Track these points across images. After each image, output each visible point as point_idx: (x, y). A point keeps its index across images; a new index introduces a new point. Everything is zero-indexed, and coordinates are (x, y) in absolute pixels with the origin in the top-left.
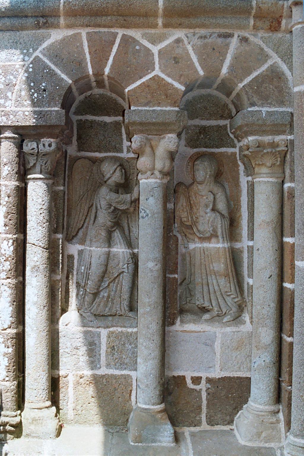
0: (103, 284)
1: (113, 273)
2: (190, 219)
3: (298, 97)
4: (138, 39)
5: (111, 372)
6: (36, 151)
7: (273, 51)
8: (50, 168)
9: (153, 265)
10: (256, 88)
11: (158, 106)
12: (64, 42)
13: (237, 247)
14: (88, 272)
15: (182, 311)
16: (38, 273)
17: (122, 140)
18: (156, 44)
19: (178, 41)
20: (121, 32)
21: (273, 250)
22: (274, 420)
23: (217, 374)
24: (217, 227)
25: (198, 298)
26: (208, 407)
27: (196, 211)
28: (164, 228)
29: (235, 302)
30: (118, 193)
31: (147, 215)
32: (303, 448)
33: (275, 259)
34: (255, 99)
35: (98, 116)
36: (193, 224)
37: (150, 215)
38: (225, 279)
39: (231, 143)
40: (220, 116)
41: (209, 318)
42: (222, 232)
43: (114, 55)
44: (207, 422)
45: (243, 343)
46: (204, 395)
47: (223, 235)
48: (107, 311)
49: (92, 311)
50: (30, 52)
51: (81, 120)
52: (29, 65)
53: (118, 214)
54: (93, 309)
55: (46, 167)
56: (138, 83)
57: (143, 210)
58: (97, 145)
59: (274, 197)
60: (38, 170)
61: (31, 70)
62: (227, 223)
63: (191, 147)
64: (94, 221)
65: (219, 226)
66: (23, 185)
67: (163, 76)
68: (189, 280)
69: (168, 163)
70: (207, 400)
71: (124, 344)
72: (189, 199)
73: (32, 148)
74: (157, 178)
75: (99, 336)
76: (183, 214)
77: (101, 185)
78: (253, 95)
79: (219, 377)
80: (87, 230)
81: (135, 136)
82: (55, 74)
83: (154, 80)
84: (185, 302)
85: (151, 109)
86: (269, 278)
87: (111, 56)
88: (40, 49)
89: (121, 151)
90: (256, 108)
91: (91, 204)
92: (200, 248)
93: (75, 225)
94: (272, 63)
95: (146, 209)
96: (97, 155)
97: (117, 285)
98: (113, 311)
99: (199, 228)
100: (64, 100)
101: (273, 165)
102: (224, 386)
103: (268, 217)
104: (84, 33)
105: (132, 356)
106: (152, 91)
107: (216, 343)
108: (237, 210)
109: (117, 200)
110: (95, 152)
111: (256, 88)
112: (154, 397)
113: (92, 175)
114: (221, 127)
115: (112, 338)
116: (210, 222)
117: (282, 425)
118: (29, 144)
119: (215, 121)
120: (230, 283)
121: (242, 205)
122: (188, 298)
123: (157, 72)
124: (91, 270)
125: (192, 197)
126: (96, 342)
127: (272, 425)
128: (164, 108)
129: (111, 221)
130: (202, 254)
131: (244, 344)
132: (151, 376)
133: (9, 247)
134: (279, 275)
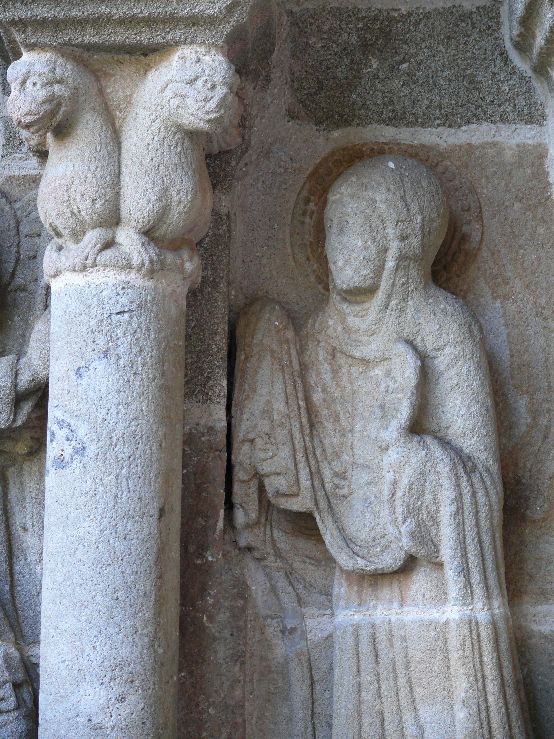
9: (102, 701)
24: (435, 520)
27: (335, 441)
28: (162, 512)
31: (81, 451)
36: (323, 504)
37: (91, 450)
39: (521, 101)
42: (462, 543)
47: (465, 556)
57: (61, 424)
62: (489, 498)
65: (446, 511)
69: (182, 192)
72: (301, 380)
74: (128, 266)
76: (271, 454)
81: (27, 57)
92: (357, 628)
95: (73, 422)
108: (546, 437)
114: (466, 17)
116: (399, 494)
125: (319, 374)
130: (367, 662)
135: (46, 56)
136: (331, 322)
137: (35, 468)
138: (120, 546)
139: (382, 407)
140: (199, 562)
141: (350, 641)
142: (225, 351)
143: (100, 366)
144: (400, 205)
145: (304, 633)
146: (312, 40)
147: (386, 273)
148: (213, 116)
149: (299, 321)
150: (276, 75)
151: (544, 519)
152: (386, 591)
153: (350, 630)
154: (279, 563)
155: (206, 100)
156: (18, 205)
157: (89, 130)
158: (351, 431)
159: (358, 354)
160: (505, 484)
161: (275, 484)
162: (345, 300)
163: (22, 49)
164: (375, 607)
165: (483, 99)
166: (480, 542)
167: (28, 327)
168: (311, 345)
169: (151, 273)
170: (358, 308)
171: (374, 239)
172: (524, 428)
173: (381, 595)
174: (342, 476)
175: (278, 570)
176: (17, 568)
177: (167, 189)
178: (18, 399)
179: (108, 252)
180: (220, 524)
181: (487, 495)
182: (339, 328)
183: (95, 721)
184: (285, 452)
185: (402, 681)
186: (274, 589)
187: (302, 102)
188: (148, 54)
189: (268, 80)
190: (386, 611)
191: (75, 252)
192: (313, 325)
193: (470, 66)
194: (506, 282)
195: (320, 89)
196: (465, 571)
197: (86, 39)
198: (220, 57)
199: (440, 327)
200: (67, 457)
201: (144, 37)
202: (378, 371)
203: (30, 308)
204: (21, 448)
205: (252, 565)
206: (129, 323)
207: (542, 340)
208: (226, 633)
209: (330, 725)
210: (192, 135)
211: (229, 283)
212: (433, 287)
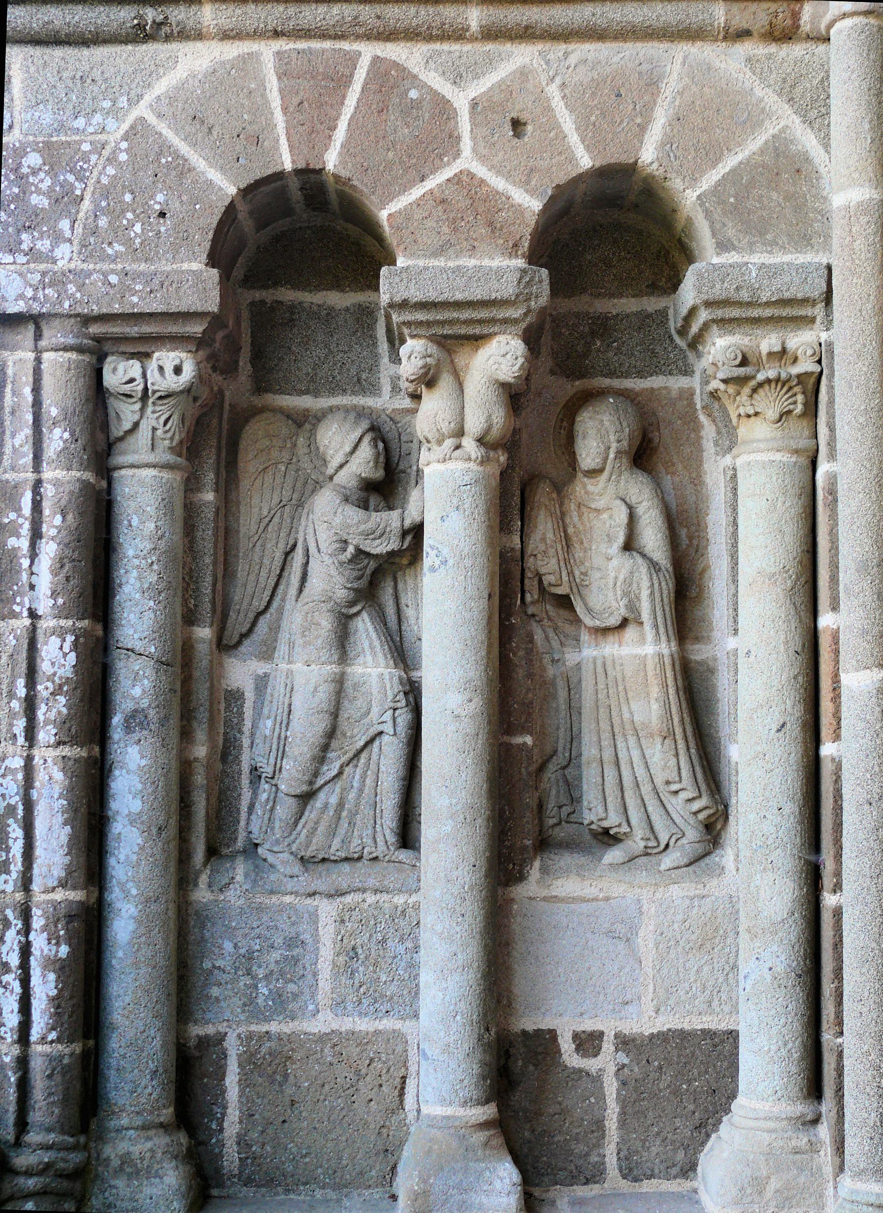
0: (326, 768)
1: (352, 737)
2: (565, 578)
3: (842, 221)
4: (415, 71)
5: (346, 1024)
6: (140, 387)
7: (780, 95)
8: (177, 434)
9: (460, 702)
10: (732, 200)
11: (470, 256)
12: (216, 79)
13: (698, 658)
14: (283, 736)
15: (543, 844)
16: (145, 732)
17: (376, 357)
18: (462, 79)
19: (523, 74)
20: (367, 52)
21: (786, 650)
22: (802, 1141)
23: (645, 1021)
24: (638, 598)
25: (589, 803)
26: (623, 1123)
28: (490, 595)
29: (695, 814)
30: (366, 508)
32: (879, 1206)
33: (795, 678)
34: (731, 232)
35: (311, 292)
36: (575, 590)
37: (451, 562)
38: (662, 744)
39: (680, 363)
40: (647, 286)
41: (622, 861)
43: (349, 116)
44: (621, 1172)
45: (716, 930)
46: (611, 1088)
47: (655, 618)
48: (336, 849)
49: (294, 848)
50: (121, 105)
51: (263, 302)
52: (117, 143)
53: (366, 567)
54: (298, 841)
55: (166, 432)
56: (416, 192)
57: (432, 548)
58: (308, 374)
59: (788, 504)
60: (145, 442)
61: (123, 157)
62: (668, 586)
63: (568, 377)
64: (301, 590)
65: (645, 594)
66: (104, 484)
67: (481, 171)
68: (567, 755)
69: (499, 417)
70: (622, 1101)
71: (384, 941)
72: (561, 519)
73: (127, 378)
74: (470, 459)
75: (313, 917)
77: (318, 485)
78: (725, 220)
79: (651, 1031)
80: (279, 619)
82: (189, 170)
83: (457, 184)
84: (554, 821)
85: (451, 264)
86: (779, 731)
87: (342, 117)
88: (148, 98)
89: (373, 389)
90: (733, 257)
91: (291, 542)
92: (595, 659)
93: (245, 603)
94: (776, 131)
95: (439, 547)
96: (306, 402)
97: (365, 772)
98: (353, 845)
99: (591, 604)
100: (215, 241)
101: (785, 415)
102: (665, 1058)
103: (772, 560)
104: (267, 51)
105: (407, 976)
106: (452, 215)
107: (641, 933)
108: (697, 551)
109: (362, 527)
110: (301, 393)
111: (732, 200)
112: (466, 1081)
113: (294, 460)
115: (349, 925)
116: (619, 584)
117: (826, 1157)
118: (121, 367)
119: (633, 300)
120: (677, 755)
121: (710, 536)
122: (564, 808)
123: (467, 160)
124: (290, 728)
125: (571, 517)
126: (306, 937)
127: (798, 1156)
128: (486, 262)
129: (345, 588)
131: (721, 932)
132: (458, 1018)
133: (65, 655)
134: (804, 725)
135: (422, 342)
136: (577, 489)
137: (412, 572)
138: (468, 615)
139: (608, 535)
140: (507, 623)
141: (591, 666)
142: (519, 506)
143: (454, 515)
144: (617, 423)
145: (564, 662)
146: (563, 330)
147: (609, 461)
148: (516, 375)
149: (560, 489)
150: (543, 350)
151: (697, 597)
152: (611, 638)
153: (591, 660)
154: (550, 623)
155: (513, 366)
156: (399, 425)
157: (446, 382)
158: (590, 549)
159: (593, 506)
160: (676, 578)
161: (548, 579)
162: (585, 476)
163: (408, 338)
164: (605, 647)
165: (659, 362)
166: (664, 610)
167: (406, 493)
168: (566, 501)
169: (482, 463)
170: (592, 480)
171: (603, 442)
172: (684, 547)
173: (608, 641)
174: (585, 574)
175: (549, 627)
176: (403, 628)
177: (490, 416)
178: (404, 533)
179: (458, 451)
180: (519, 602)
181: (667, 584)
182: (583, 492)
183: (456, 713)
184: (554, 561)
185: (621, 688)
186: (547, 638)
187: (557, 365)
188: (477, 340)
189: (539, 353)
190: (610, 649)
191: (438, 452)
192: (567, 491)
194: (673, 465)
195: (568, 358)
197: (445, 332)
198: (520, 341)
199: (639, 490)
200: (437, 567)
201: (477, 330)
202: (605, 516)
203: (407, 483)
204: (405, 561)
205: (534, 624)
206: (470, 491)
207: (694, 497)
208: (523, 662)
209: (580, 713)
210: (504, 385)
211: (520, 467)
212: (635, 468)
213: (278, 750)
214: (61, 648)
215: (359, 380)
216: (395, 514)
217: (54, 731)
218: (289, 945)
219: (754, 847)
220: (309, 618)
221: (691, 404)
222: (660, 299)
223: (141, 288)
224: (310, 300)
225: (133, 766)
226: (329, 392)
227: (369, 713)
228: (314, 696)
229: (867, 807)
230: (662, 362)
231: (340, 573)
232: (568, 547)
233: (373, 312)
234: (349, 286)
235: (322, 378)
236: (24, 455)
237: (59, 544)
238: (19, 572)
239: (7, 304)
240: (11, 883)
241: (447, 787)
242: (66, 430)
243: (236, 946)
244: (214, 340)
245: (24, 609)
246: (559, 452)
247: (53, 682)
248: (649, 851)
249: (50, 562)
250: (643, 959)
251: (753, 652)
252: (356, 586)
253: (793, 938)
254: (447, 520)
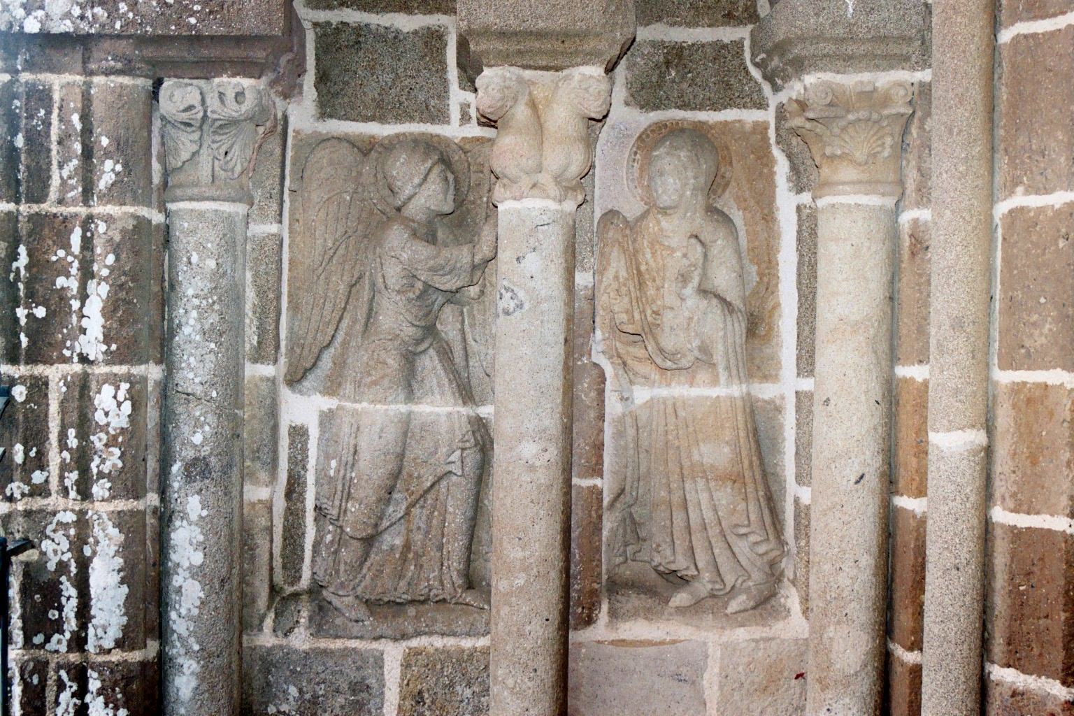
6: (201, 114)
17: (445, 83)
21: (867, 400)
31: (520, 306)
35: (378, 13)
37: (527, 306)
39: (755, 96)
40: (724, 16)
54: (363, 584)
58: (373, 100)
59: (873, 249)
71: (452, 685)
86: (857, 482)
89: (441, 116)
91: (356, 275)
107: (706, 676)
108: (767, 289)
114: (724, 46)
119: (709, 29)
125: (644, 255)
126: (372, 681)
133: (119, 404)
159: (667, 244)
183: (530, 463)
187: (632, 95)
193: (726, 75)
196: (728, 368)
200: (511, 310)
213: (342, 492)
214: (115, 397)
215: (427, 107)
216: (465, 249)
217: (108, 485)
218: (354, 690)
219: (828, 598)
220: (376, 357)
221: (765, 138)
222: (737, 29)
223: (199, 8)
224: (377, 22)
225: (194, 517)
226: (396, 119)
227: (436, 453)
228: (380, 437)
229: (954, 572)
230: (737, 94)
231: (407, 310)
232: (640, 284)
233: (442, 36)
234: (418, 7)
235: (388, 104)
236: (73, 188)
237: (111, 286)
238: (70, 313)
239: (52, 24)
240: (65, 643)
241: (520, 539)
242: (118, 162)
243: (300, 691)
244: (278, 65)
245: (75, 355)
246: (632, 185)
247: (107, 433)
248: (716, 593)
249: (101, 305)
250: (708, 701)
251: (832, 401)
252: (424, 324)
253: (865, 690)
254: (522, 261)
